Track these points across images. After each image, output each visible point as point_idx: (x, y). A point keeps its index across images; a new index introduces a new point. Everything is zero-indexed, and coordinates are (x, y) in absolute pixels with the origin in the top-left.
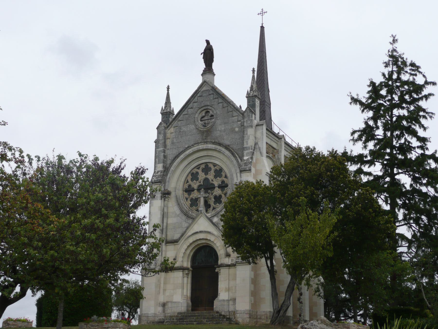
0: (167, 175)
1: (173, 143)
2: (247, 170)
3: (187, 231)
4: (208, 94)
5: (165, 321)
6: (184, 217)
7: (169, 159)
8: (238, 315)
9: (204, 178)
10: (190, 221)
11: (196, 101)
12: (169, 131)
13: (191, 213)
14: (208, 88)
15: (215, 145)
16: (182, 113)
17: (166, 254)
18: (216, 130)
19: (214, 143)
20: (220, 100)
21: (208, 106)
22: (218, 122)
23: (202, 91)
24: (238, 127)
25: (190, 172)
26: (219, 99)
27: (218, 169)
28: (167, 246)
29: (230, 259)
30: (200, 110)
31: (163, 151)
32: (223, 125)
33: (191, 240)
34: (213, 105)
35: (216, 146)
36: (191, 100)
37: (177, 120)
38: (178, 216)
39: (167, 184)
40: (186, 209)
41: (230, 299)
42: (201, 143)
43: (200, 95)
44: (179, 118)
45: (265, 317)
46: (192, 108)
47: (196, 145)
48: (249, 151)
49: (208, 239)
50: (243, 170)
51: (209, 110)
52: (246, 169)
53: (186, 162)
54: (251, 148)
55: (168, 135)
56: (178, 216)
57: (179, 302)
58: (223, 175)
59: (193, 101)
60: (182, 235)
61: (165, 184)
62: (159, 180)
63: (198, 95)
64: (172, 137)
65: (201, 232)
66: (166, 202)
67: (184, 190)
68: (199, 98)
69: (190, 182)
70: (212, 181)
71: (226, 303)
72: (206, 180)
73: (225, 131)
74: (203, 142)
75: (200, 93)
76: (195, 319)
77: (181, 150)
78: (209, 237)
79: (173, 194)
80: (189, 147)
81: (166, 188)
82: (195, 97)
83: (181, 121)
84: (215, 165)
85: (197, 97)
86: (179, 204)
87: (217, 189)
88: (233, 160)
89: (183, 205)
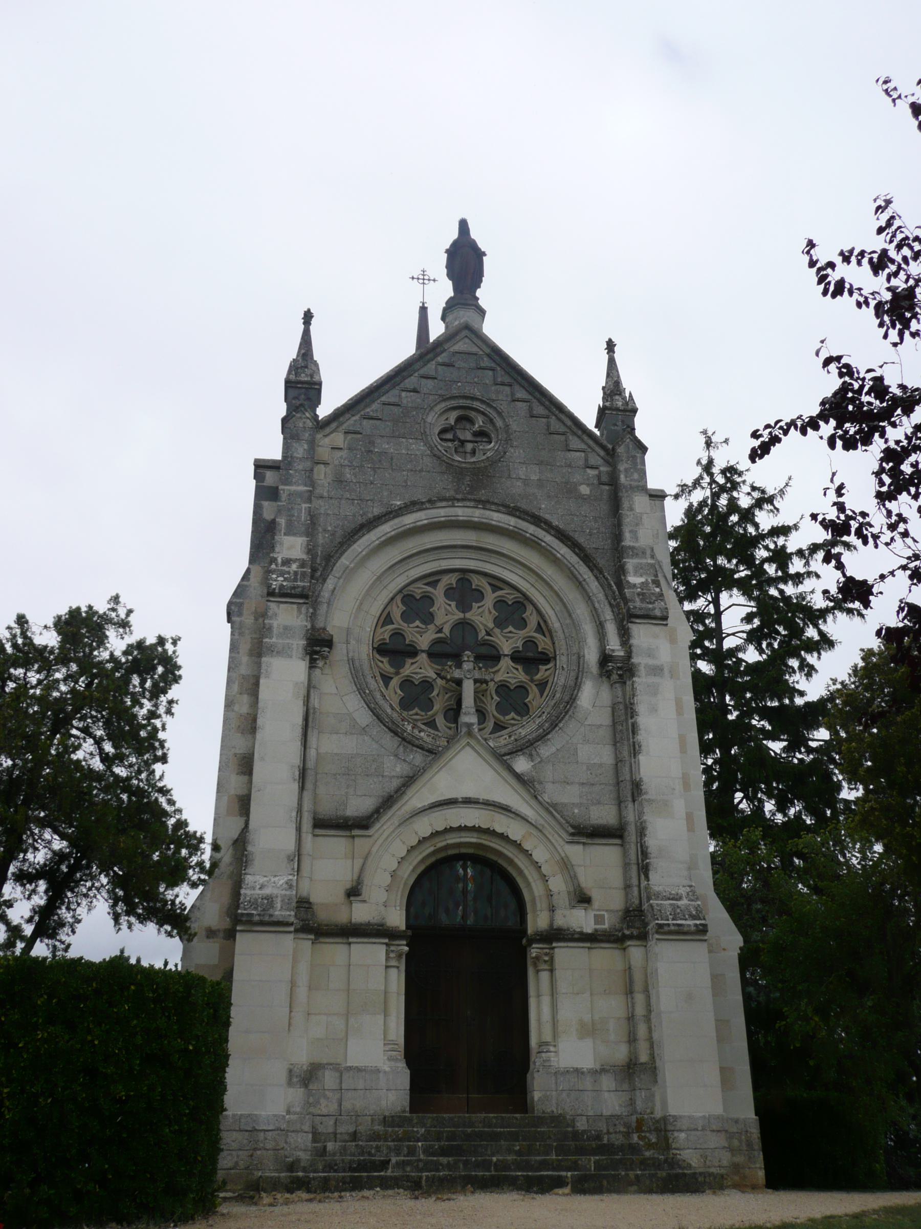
0: (325, 580)
1: (339, 481)
2: (655, 618)
3: (410, 792)
4: (473, 365)
5: (394, 1160)
6: (389, 741)
7: (325, 530)
8: (683, 1135)
9: (456, 617)
10: (417, 758)
11: (433, 373)
12: (327, 441)
13: (409, 728)
14: (475, 349)
15: (519, 517)
16: (379, 397)
17: (625, 854)
18: (509, 477)
19: (515, 511)
20: (521, 394)
21: (473, 398)
22: (516, 454)
23: (452, 350)
24: (588, 485)
25: (400, 591)
26: (516, 387)
27: (510, 599)
28: (356, 840)
29: (591, 914)
30: (443, 405)
31: (307, 495)
32: (536, 468)
33: (424, 826)
34: (494, 400)
35: (520, 521)
36: (416, 366)
37: (359, 412)
38: (364, 730)
39: (323, 609)
40: (389, 711)
41: (598, 1067)
42: (463, 500)
43: (447, 360)
44: (368, 410)
45: (740, 1141)
46: (415, 391)
47: (444, 504)
48: (644, 561)
49: (499, 830)
50: (639, 613)
51: (473, 414)
52: (651, 613)
53: (395, 553)
54: (648, 552)
55: (323, 452)
56: (364, 730)
57: (378, 1071)
58: (533, 620)
59: (422, 372)
60: (388, 802)
61: (315, 609)
62: (304, 587)
63: (439, 359)
64: (336, 462)
65: (468, 801)
66: (317, 672)
67: (375, 646)
68: (440, 368)
69: (398, 622)
70: (488, 634)
71: (588, 1083)
72: (463, 626)
73: (540, 484)
74: (470, 500)
75: (444, 355)
76: (519, 1153)
77: (377, 511)
78: (501, 824)
79: (340, 652)
80: (412, 506)
81: (320, 624)
82: (429, 361)
83: (376, 421)
84: (497, 583)
85: (434, 362)
86: (362, 690)
87: (506, 663)
88: (586, 577)
89: (378, 696)
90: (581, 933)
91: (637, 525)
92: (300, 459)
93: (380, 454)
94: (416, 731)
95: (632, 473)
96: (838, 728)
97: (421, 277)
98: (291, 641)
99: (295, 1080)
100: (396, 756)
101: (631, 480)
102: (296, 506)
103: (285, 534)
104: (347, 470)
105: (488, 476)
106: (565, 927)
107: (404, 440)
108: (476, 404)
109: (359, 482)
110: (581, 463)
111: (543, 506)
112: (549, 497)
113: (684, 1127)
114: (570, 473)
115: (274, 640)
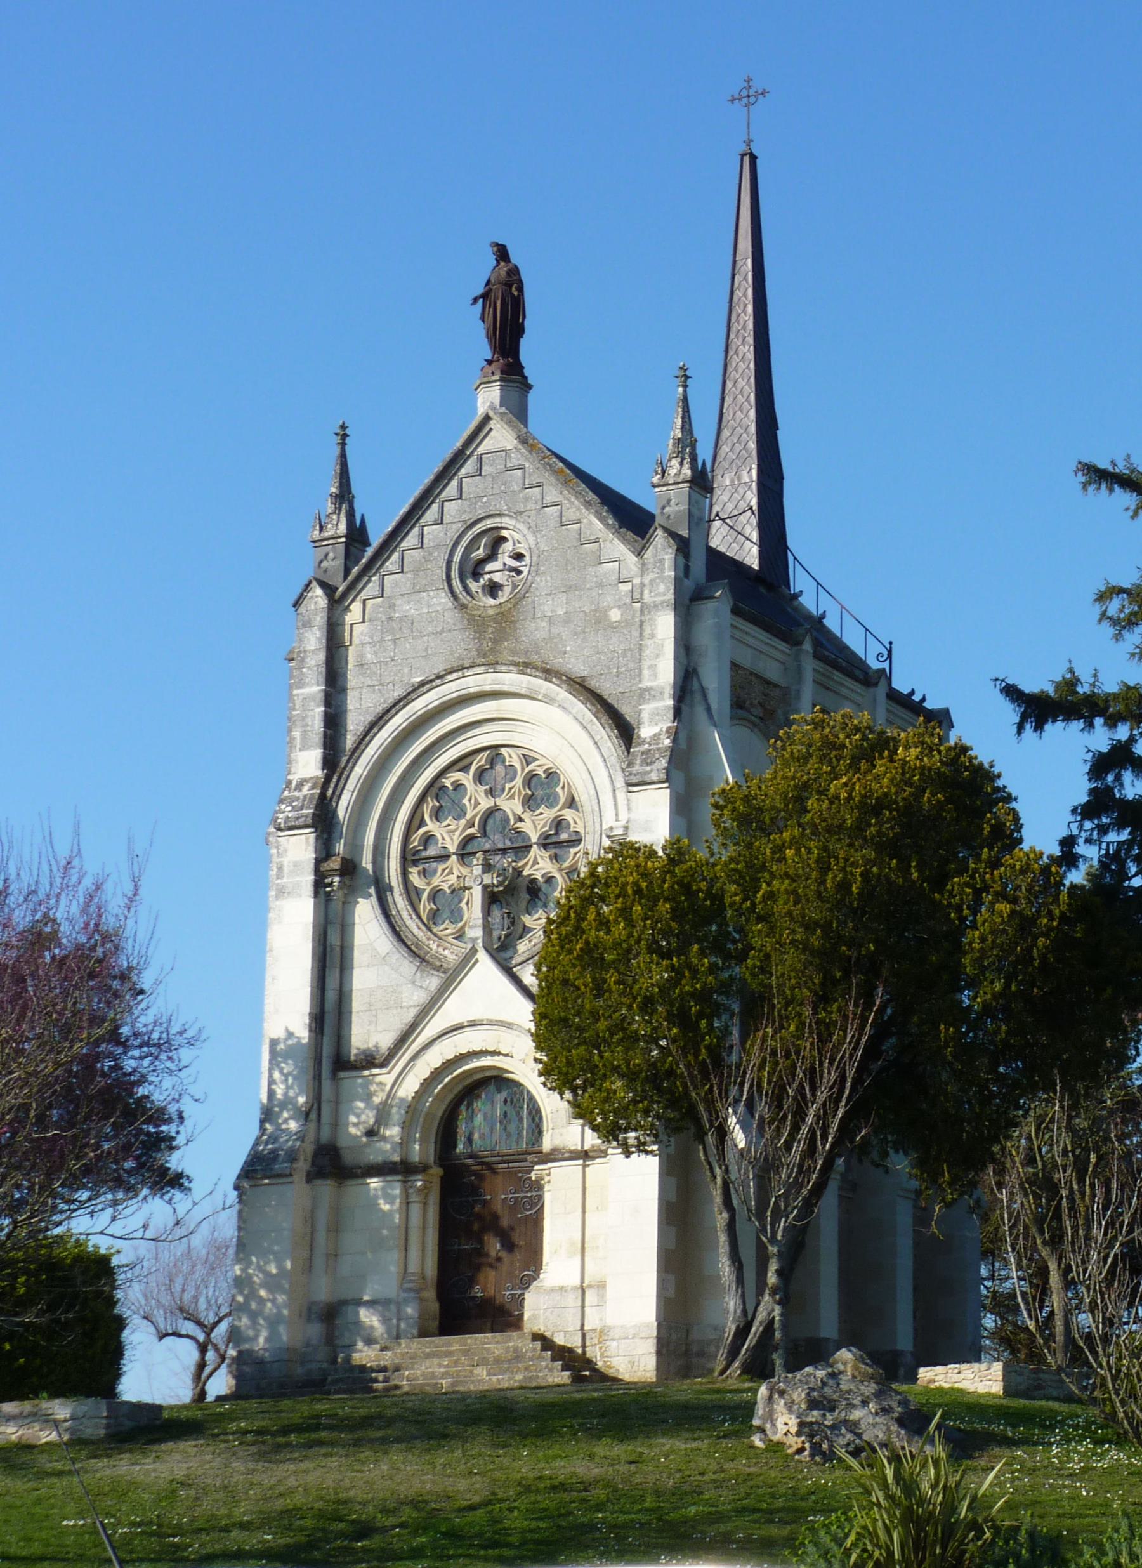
8: (614, 1344)
10: (433, 982)
24: (619, 607)
32: (563, 597)
73: (567, 620)
76: (447, 1366)
77: (397, 693)
90: (571, 1152)
91: (657, 656)
92: (313, 651)
93: (401, 619)
94: (440, 949)
95: (658, 585)
96: (914, 864)
97: (752, 92)
98: (298, 879)
99: (313, 1316)
100: (414, 983)
101: (656, 595)
102: (310, 713)
103: (300, 750)
104: (368, 648)
105: (512, 622)
106: (561, 1146)
107: (424, 594)
108: (457, 557)
109: (379, 662)
110: (614, 577)
111: (568, 649)
112: (575, 634)
113: (616, 1337)
114: (600, 595)
115: (285, 880)
